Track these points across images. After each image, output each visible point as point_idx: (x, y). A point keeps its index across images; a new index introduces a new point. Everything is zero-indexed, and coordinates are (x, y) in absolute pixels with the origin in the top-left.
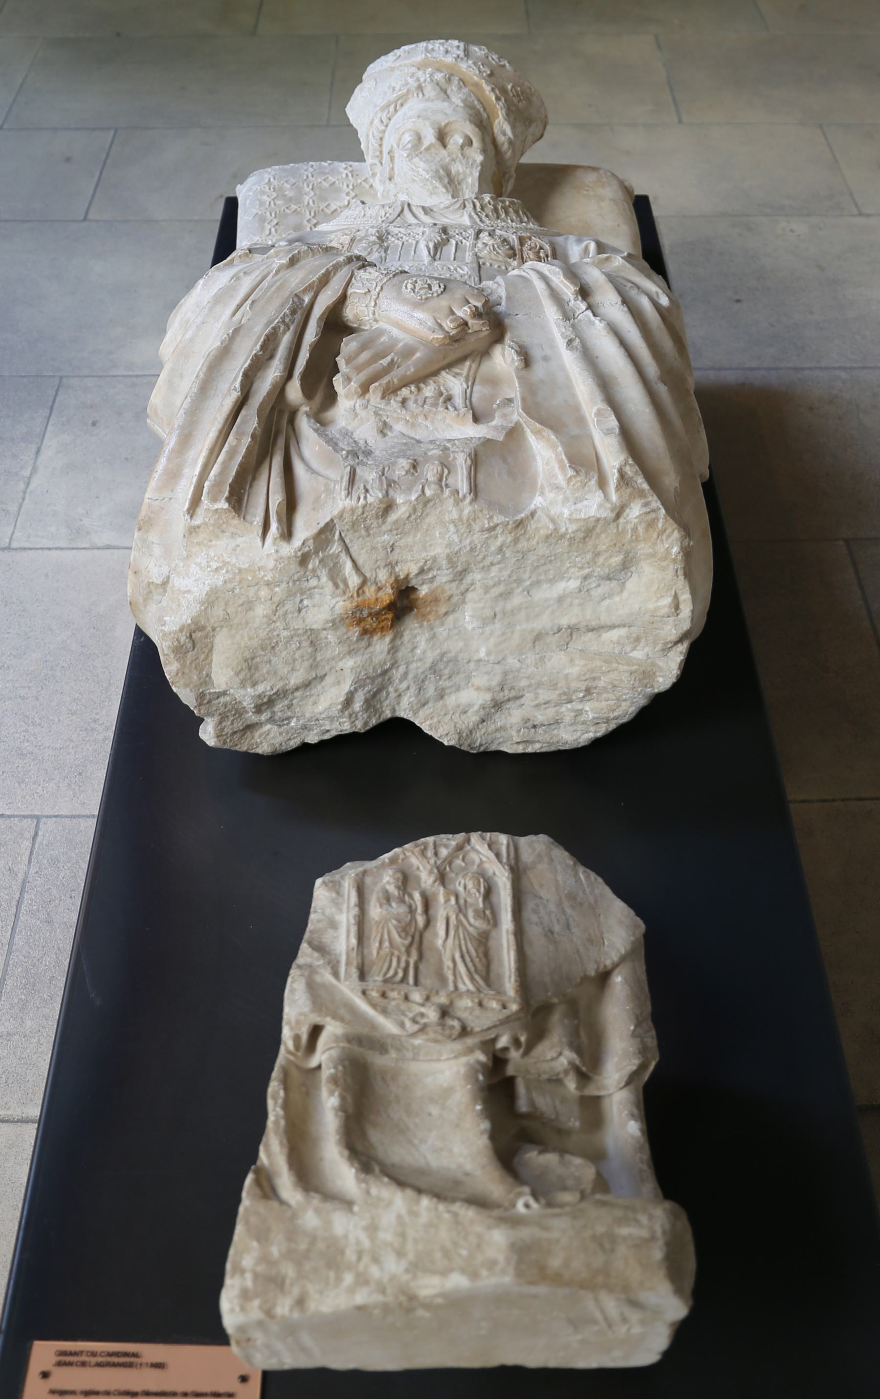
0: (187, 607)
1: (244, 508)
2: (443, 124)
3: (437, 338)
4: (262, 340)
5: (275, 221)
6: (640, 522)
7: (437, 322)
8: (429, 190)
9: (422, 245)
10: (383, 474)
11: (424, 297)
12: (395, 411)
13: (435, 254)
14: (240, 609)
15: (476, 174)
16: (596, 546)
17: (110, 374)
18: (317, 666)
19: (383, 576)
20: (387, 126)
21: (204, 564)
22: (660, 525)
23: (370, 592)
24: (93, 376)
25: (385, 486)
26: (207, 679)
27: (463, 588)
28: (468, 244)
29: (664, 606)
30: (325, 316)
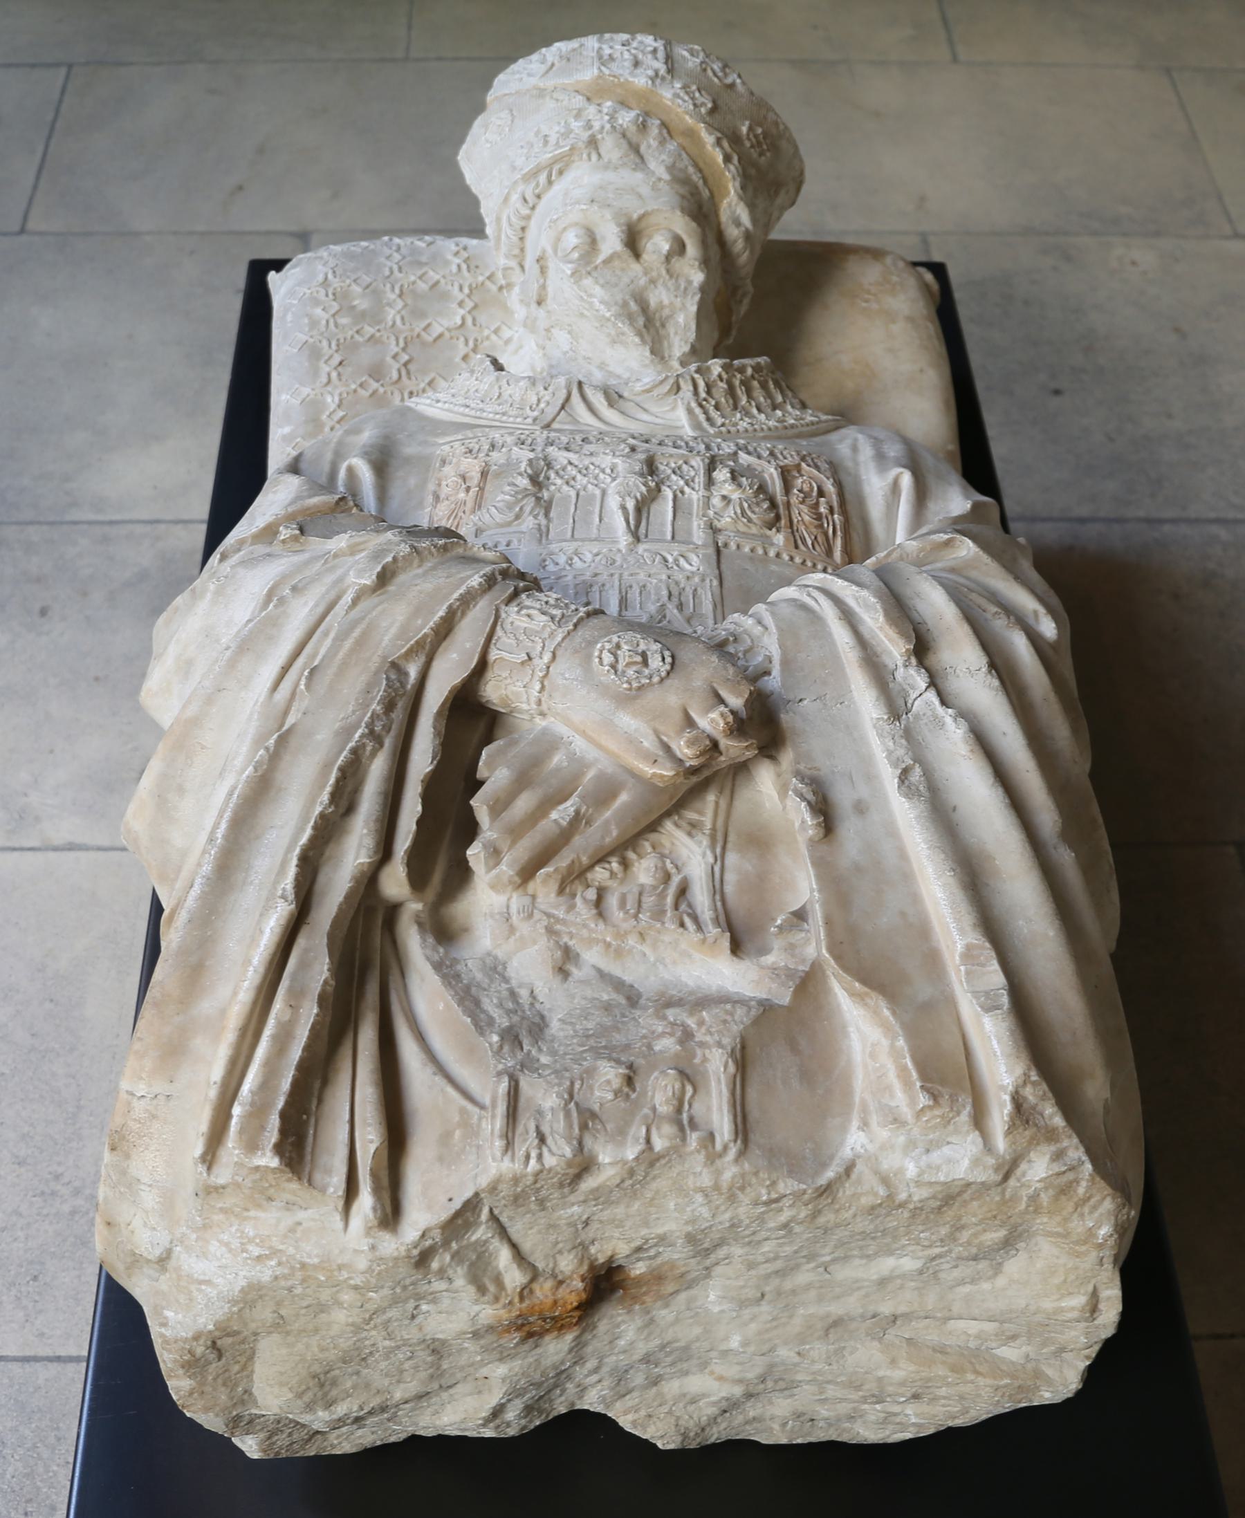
0: (206, 1305)
1: (308, 1157)
2: (635, 216)
3: (662, 776)
4: (332, 780)
5: (337, 359)
6: (1046, 1188)
7: (661, 741)
8: (609, 335)
9: (613, 502)
10: (571, 1097)
11: (635, 685)
12: (585, 926)
13: (638, 526)
14: (303, 1311)
15: (693, 308)
16: (960, 1219)
17: (68, 518)
18: (441, 1375)
19: (567, 1264)
20: (533, 208)
21: (235, 1244)
22: (1081, 1191)
23: (543, 1290)
24: (39, 523)
25: (577, 1131)
26: (246, 1397)
27: (708, 1263)
28: (695, 496)
29: (1073, 1309)
30: (448, 705)
